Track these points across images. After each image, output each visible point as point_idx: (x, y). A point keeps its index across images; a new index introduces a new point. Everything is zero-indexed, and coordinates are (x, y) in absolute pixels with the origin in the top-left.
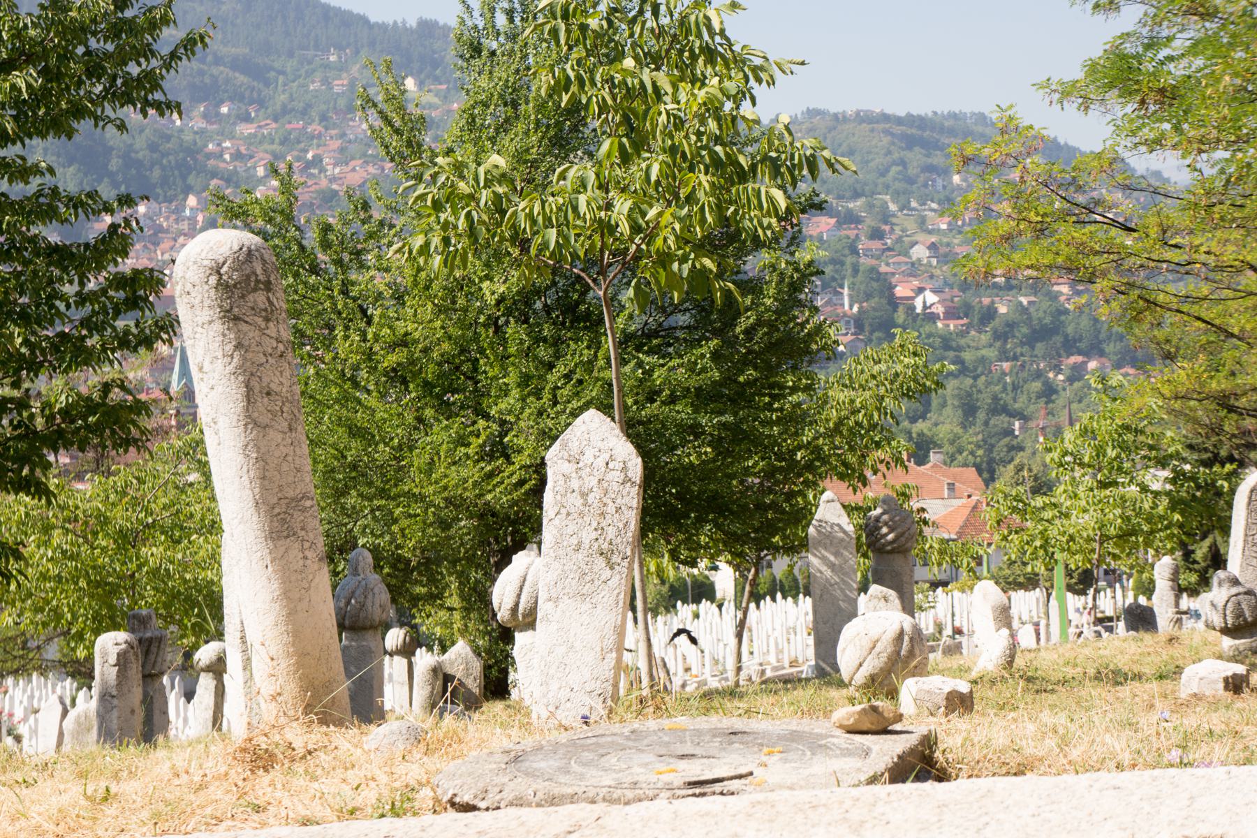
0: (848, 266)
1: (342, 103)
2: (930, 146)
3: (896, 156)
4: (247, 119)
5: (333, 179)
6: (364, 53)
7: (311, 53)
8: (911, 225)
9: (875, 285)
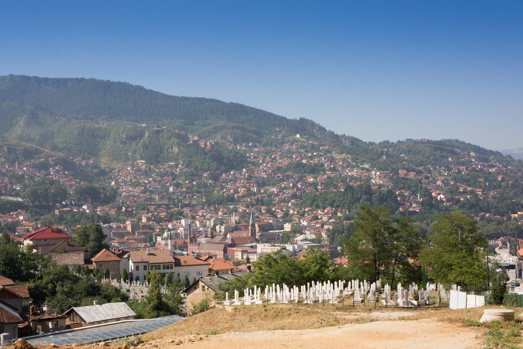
0: (419, 187)
1: (280, 142)
2: (442, 150)
3: (432, 153)
4: (256, 147)
5: (279, 164)
6: (286, 127)
7: (272, 128)
8: (437, 174)
9: (427, 193)
